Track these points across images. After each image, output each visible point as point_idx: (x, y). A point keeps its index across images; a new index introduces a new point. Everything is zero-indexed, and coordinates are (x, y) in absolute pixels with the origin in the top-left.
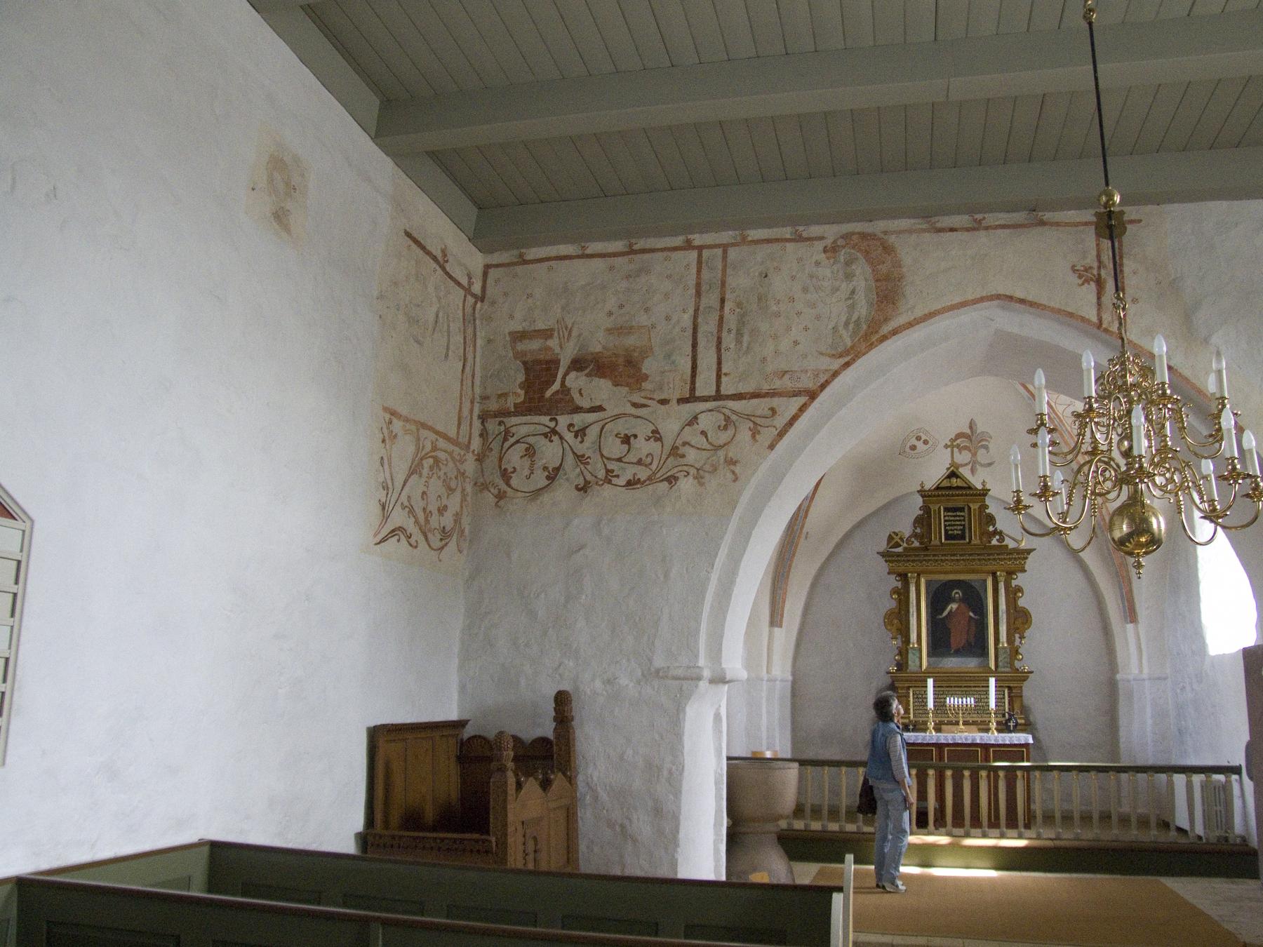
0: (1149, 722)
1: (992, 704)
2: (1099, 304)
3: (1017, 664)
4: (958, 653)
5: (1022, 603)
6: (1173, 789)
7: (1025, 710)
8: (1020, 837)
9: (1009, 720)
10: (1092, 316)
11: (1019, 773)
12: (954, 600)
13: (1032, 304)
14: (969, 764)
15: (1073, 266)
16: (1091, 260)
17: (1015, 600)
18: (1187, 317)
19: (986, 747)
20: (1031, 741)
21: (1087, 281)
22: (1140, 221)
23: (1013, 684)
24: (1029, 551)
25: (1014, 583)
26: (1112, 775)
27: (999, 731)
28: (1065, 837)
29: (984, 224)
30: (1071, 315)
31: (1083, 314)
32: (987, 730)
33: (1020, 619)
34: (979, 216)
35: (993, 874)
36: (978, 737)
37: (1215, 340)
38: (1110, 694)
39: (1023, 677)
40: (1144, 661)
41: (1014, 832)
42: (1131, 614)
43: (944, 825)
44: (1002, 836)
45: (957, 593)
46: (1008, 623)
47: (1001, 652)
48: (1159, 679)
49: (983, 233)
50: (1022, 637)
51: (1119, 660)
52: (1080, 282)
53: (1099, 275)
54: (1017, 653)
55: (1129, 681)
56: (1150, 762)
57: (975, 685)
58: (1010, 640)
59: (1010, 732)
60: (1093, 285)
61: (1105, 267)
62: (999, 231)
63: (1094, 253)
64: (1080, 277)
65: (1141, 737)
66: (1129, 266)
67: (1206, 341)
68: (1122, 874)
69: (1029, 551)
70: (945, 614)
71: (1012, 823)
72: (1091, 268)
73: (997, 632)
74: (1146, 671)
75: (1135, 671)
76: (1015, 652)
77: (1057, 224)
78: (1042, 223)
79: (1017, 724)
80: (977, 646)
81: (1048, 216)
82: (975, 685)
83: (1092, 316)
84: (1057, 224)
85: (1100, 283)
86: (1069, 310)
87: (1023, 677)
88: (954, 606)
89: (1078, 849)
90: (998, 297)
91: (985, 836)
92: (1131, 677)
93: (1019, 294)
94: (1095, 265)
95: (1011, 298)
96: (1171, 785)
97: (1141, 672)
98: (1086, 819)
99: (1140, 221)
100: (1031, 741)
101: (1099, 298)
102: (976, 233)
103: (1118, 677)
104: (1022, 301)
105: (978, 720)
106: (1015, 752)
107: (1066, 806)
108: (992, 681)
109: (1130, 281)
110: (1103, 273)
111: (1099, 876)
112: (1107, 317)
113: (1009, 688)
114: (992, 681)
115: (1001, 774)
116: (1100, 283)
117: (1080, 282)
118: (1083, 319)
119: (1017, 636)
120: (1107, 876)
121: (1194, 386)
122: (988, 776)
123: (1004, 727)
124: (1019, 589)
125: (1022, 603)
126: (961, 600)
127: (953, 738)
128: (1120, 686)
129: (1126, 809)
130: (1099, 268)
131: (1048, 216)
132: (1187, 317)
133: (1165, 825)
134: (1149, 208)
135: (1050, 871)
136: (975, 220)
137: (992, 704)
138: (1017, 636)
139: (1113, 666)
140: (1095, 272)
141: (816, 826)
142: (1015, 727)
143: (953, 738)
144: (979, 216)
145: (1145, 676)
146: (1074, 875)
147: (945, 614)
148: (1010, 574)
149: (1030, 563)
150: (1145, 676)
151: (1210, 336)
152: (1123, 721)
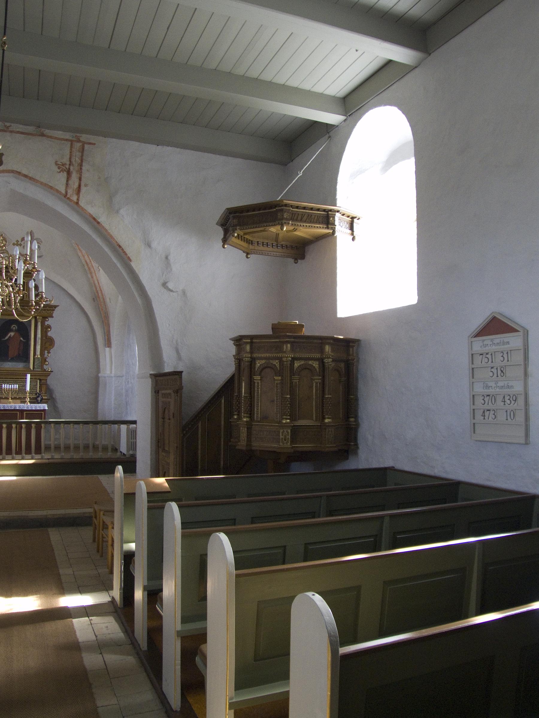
0: (113, 398)
1: (28, 388)
2: (67, 184)
3: (45, 367)
4: (13, 360)
5: (49, 334)
6: (120, 431)
7: (49, 391)
8: (32, 459)
9: (38, 397)
10: (63, 190)
11: (33, 425)
12: (12, 331)
13: (31, 178)
14: (6, 421)
15: (56, 162)
16: (66, 160)
17: (46, 332)
18: (110, 199)
19: (22, 411)
20: (47, 408)
21: (62, 171)
22: (95, 144)
23: (42, 377)
24: (56, 307)
25: (46, 323)
26: (91, 426)
27: (31, 402)
28: (65, 457)
29: (11, 129)
30: (51, 188)
31: (58, 188)
32: (25, 402)
33: (48, 343)
34: (8, 124)
35: (14, 478)
36: (18, 406)
37: (122, 211)
38: (95, 383)
39: (48, 374)
40: (113, 368)
41: (29, 456)
42: (108, 343)
43: (21, 454)
44: (23, 459)
45: (14, 327)
46: (41, 344)
47: (36, 360)
48: (119, 376)
49: (8, 134)
50: (49, 353)
51: (101, 367)
52: (59, 171)
53: (69, 168)
54: (45, 361)
55: (105, 377)
56: (112, 419)
57: (19, 378)
58: (42, 354)
59: (38, 403)
60: (65, 174)
61: (73, 165)
62: (18, 135)
63: (68, 156)
64: (59, 168)
65: (108, 407)
66: (85, 167)
67: (117, 212)
68: (81, 475)
69: (56, 307)
70: (7, 338)
71: (28, 451)
72: (65, 164)
73: (35, 349)
74: (113, 372)
75: (108, 372)
76: (44, 360)
77: (51, 137)
78: (43, 135)
79: (42, 399)
80: (24, 356)
81: (47, 132)
82: (19, 378)
83: (63, 190)
84: (51, 137)
85: (69, 173)
86: (50, 184)
87: (48, 374)
88: (12, 334)
89: (64, 463)
90: (13, 172)
91: (13, 459)
92: (106, 375)
93: (25, 172)
94: (68, 163)
95: (19, 173)
96: (119, 430)
97: (111, 373)
98: (77, 448)
99: (95, 144)
100: (47, 408)
101: (67, 181)
102: (5, 133)
103: (100, 375)
104: (26, 176)
105: (20, 396)
106: (39, 414)
107: (48, 443)
108: (29, 376)
109: (85, 175)
110: (71, 168)
111: (70, 476)
112: (70, 192)
113: (40, 380)
114: (29, 376)
115: (23, 426)
116: (69, 173)
117: (59, 171)
118: (57, 191)
119: (46, 351)
120: (75, 476)
121: (109, 233)
122: (16, 427)
123: (34, 401)
124: (49, 327)
125: (49, 334)
126: (16, 331)
127: (4, 407)
128: (101, 379)
129: (104, 442)
130: (70, 165)
131: (47, 132)
132: (110, 199)
133: (115, 450)
134: (101, 138)
135: (46, 475)
136: (5, 126)
137: (28, 388)
138: (46, 351)
139: (98, 370)
140: (67, 167)
141: (57, 456)
142: (41, 400)
143: (4, 407)
144: (8, 124)
145: (113, 375)
146: (57, 477)
147: (7, 338)
148: (45, 318)
149: (55, 313)
150: (113, 375)
151: (120, 209)
152: (101, 398)
